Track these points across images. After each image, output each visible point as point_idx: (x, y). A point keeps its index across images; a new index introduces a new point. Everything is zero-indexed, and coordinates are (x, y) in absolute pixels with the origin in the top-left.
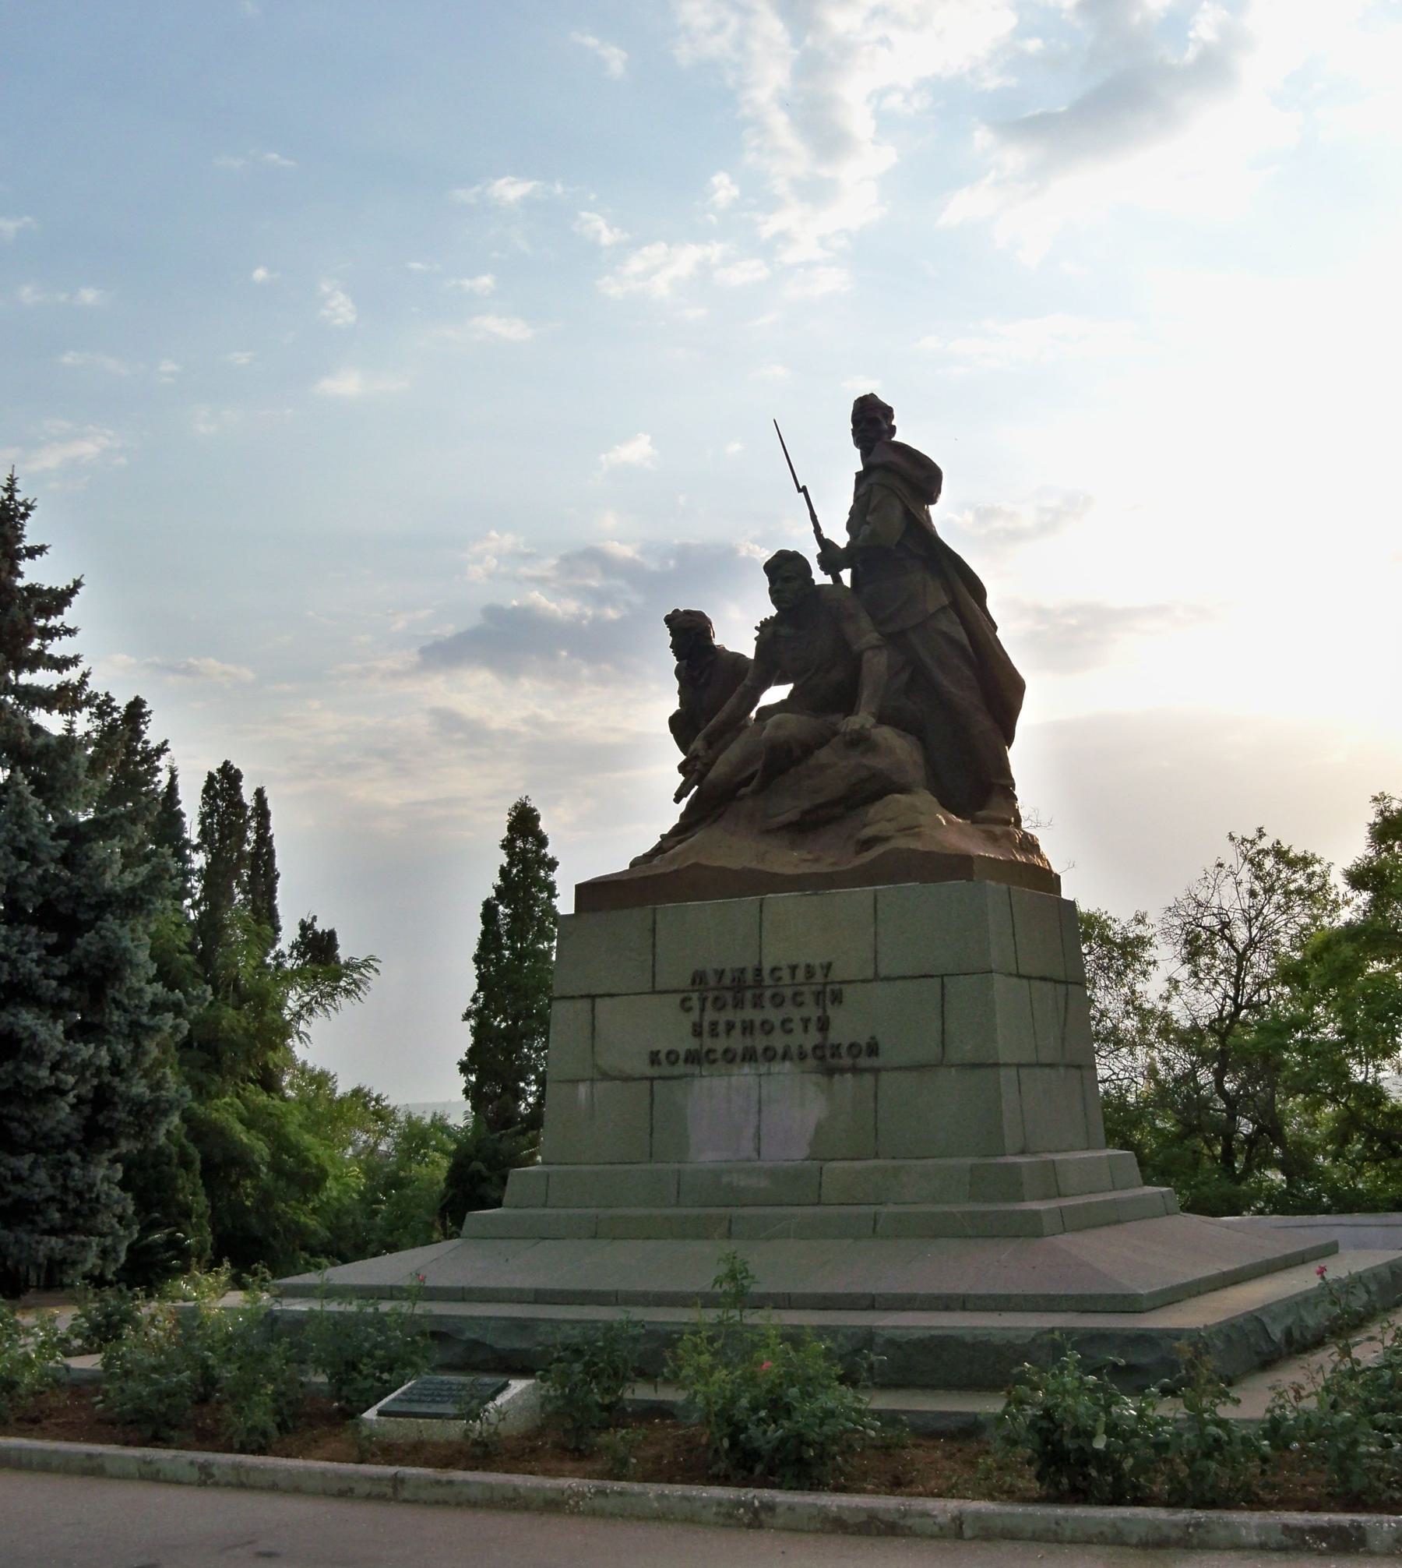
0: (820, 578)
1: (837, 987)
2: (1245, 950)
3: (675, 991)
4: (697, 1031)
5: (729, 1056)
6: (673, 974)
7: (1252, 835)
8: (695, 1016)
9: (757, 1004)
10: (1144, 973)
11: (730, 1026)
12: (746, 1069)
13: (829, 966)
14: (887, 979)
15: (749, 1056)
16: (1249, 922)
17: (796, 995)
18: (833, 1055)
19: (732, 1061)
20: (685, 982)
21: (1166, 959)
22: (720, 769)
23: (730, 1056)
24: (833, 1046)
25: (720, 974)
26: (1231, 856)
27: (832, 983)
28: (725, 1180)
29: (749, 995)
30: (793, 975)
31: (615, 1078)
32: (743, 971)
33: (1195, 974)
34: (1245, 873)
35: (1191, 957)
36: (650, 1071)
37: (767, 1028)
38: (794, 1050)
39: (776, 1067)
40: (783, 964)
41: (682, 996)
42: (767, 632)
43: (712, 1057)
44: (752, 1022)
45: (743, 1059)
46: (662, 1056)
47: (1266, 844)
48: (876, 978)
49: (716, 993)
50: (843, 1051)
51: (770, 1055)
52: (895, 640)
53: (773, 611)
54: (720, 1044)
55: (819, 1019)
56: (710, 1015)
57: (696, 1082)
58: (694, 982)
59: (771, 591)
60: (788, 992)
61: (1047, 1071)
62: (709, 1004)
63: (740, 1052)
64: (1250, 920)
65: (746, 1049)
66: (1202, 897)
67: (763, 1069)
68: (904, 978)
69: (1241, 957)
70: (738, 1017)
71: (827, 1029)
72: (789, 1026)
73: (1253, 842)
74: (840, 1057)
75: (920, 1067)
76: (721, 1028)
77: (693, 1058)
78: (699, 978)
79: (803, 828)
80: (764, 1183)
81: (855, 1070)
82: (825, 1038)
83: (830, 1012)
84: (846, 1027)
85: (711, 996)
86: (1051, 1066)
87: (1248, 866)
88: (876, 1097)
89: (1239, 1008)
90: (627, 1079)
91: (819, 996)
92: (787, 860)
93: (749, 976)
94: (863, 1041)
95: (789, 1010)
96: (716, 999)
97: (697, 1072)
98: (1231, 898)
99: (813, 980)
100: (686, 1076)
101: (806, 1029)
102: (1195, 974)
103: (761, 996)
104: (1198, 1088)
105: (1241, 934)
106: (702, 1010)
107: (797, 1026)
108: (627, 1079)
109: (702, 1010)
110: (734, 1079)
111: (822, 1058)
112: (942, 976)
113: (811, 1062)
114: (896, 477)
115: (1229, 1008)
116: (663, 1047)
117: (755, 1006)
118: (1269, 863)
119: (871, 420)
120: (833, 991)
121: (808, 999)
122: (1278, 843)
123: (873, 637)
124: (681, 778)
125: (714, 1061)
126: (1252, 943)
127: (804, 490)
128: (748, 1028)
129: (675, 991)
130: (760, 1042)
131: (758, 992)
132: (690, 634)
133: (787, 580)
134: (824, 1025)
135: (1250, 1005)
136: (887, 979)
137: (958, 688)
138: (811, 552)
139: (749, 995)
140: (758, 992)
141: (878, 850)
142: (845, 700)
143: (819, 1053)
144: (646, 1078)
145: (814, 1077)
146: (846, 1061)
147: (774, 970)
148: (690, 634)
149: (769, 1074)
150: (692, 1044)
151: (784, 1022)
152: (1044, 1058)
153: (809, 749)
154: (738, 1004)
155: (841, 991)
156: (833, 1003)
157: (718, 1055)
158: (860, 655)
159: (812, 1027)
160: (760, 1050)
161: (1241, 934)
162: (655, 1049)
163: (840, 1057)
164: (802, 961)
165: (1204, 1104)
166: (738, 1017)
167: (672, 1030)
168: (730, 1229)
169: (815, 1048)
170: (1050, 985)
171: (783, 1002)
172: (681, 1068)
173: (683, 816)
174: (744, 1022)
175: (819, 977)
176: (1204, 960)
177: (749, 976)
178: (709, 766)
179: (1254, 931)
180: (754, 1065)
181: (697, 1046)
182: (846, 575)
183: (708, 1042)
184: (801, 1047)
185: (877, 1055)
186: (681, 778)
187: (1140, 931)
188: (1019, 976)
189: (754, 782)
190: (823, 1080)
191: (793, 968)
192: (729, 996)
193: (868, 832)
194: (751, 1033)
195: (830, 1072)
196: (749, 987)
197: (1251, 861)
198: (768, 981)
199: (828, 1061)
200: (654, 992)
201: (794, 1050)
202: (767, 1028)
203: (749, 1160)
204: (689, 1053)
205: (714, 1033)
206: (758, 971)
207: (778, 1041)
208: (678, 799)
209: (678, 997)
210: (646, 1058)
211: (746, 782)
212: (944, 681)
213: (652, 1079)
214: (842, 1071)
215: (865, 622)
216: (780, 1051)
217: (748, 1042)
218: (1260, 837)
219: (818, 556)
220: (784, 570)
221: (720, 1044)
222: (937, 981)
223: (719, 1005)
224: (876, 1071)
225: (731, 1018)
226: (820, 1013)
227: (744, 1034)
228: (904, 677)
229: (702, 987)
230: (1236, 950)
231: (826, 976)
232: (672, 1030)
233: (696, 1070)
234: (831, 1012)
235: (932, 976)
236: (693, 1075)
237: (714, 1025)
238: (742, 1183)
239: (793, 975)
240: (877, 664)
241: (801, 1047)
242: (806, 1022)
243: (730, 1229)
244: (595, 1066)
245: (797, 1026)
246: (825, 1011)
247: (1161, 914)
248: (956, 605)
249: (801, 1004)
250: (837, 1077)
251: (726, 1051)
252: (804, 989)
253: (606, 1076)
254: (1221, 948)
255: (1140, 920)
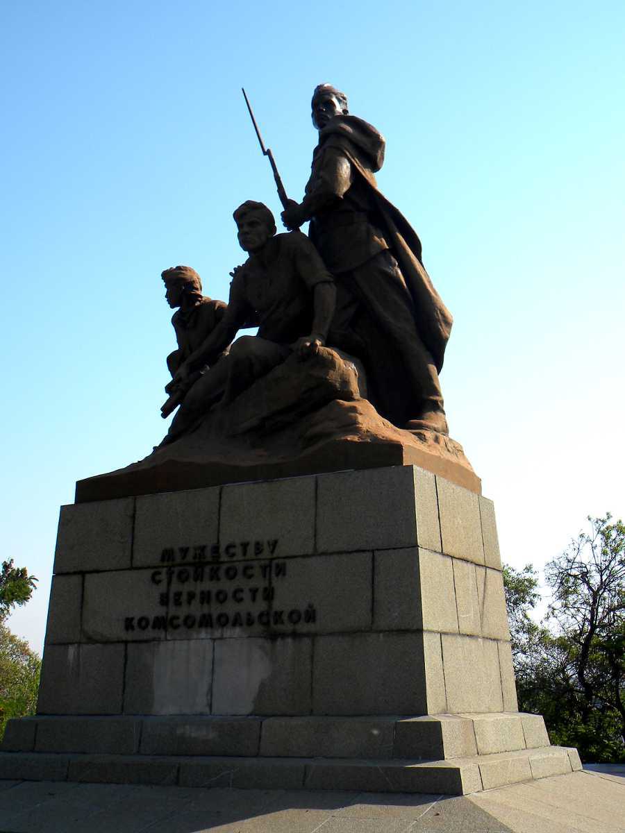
0: (281, 229)
1: (281, 561)
2: (599, 590)
3: (149, 567)
4: (164, 601)
5: (189, 623)
6: (148, 554)
7: (605, 517)
8: (163, 587)
9: (214, 576)
10: (531, 603)
11: (191, 596)
12: (203, 634)
13: (274, 544)
14: (323, 554)
15: (206, 622)
16: (601, 572)
17: (246, 568)
18: (276, 622)
19: (190, 627)
20: (155, 559)
21: (546, 592)
22: (197, 390)
23: (189, 623)
24: (276, 613)
25: (185, 551)
26: (590, 530)
27: (279, 558)
28: (179, 731)
29: (207, 569)
30: (245, 554)
31: (97, 642)
32: (203, 548)
33: (566, 606)
34: (599, 541)
35: (564, 594)
36: (125, 635)
37: (221, 597)
38: (244, 617)
39: (228, 632)
40: (238, 542)
41: (152, 571)
42: (240, 276)
43: (175, 622)
44: (209, 592)
45: (201, 626)
46: (135, 622)
47: (611, 523)
48: (316, 553)
49: (181, 568)
50: (285, 617)
51: (223, 621)
52: (344, 279)
53: (242, 257)
54: (182, 612)
55: (265, 589)
56: (176, 587)
57: (163, 647)
58: (163, 560)
59: (239, 235)
60: (240, 566)
61: (467, 640)
62: (174, 579)
63: (198, 619)
64: (601, 571)
65: (204, 616)
66: (571, 557)
67: (217, 634)
68: (340, 553)
69: (595, 595)
70: (199, 587)
71: (272, 598)
72: (239, 595)
73: (604, 522)
74: (282, 623)
75: (352, 633)
76: (184, 598)
77: (162, 623)
78: (167, 555)
79: (263, 433)
80: (212, 735)
81: (295, 635)
82: (270, 607)
83: (274, 584)
84: (288, 596)
85: (176, 570)
86: (470, 636)
87: (600, 536)
88: (312, 657)
89: (593, 627)
90: (107, 642)
91: (265, 569)
92: (247, 458)
93: (208, 554)
94: (303, 607)
95: (240, 581)
96: (180, 573)
97: (163, 636)
98: (589, 557)
99: (260, 556)
100: (154, 640)
101: (254, 599)
102: (566, 606)
103: (218, 569)
104: (567, 679)
105: (595, 580)
106: (169, 583)
107: (246, 595)
108: (107, 642)
109: (169, 583)
110: (192, 642)
111: (267, 624)
112: (373, 551)
113: (257, 628)
114: (345, 138)
115: (587, 627)
116: (136, 614)
117: (212, 579)
118: (614, 534)
119: (322, 101)
120: (277, 566)
121: (257, 571)
122: (620, 522)
123: (324, 273)
124: (167, 397)
125: (176, 627)
126: (604, 586)
127: (267, 153)
128: (206, 597)
129: (149, 567)
130: (215, 610)
131: (215, 566)
132: (179, 286)
133: (252, 224)
134: (269, 595)
135: (603, 627)
136: (323, 554)
137: (402, 326)
138: (276, 209)
139: (207, 569)
140: (215, 566)
141: (321, 444)
142: (303, 325)
143: (265, 619)
144: (122, 642)
145: (260, 641)
146: (288, 627)
147: (228, 547)
148: (179, 286)
149: (221, 638)
150: (160, 611)
151: (236, 592)
152: (466, 629)
153: (267, 367)
154: (199, 577)
155: (284, 564)
156: (277, 575)
157: (180, 621)
158: (313, 287)
159: (260, 595)
160: (215, 616)
161: (595, 580)
162: (130, 616)
163: (282, 623)
164: (252, 539)
165: (570, 689)
166: (199, 587)
167: (142, 599)
168: (177, 778)
169: (261, 615)
170: (471, 567)
171: (235, 574)
172: (150, 633)
173: (171, 429)
174: (202, 593)
175: (266, 554)
176: (571, 598)
177: (208, 554)
178: (189, 386)
179: (604, 577)
180: (209, 630)
181: (164, 614)
182: (305, 228)
183: (173, 611)
184: (249, 614)
185: (314, 621)
186: (167, 397)
187: (528, 576)
188: (442, 553)
189: (224, 398)
190: (268, 645)
191: (245, 546)
192: (191, 570)
193: (318, 429)
194: (208, 602)
195: (273, 637)
196: (208, 563)
197: (603, 533)
198: (224, 558)
199: (272, 627)
200: (132, 568)
201: (244, 617)
202: (221, 597)
203: (202, 714)
204: (157, 618)
205: (178, 603)
206: (216, 549)
207: (231, 608)
208: (165, 415)
209: (149, 573)
210: (122, 625)
211: (218, 398)
212: (388, 317)
213: (126, 642)
214: (283, 635)
215: (318, 262)
216: (231, 618)
217: (206, 610)
218: (608, 518)
219: (282, 214)
220: (250, 218)
221: (182, 612)
222: (369, 555)
223: (183, 578)
224: (313, 636)
225: (192, 589)
226: (266, 584)
227: (202, 603)
228: (351, 311)
229: (170, 563)
230: (593, 590)
231: (272, 552)
232: (142, 599)
233: (162, 634)
234: (277, 583)
235: (364, 551)
236: (159, 640)
237: (178, 595)
238: (193, 735)
239: (245, 554)
240: (328, 296)
241: (249, 614)
242: (254, 592)
243: (177, 778)
244: (82, 631)
245: (246, 595)
246: (270, 583)
247: (543, 566)
248: (396, 250)
249: (250, 577)
250: (279, 642)
251: (187, 617)
252: (255, 563)
253: (91, 640)
254: (583, 589)
255: (528, 569)
